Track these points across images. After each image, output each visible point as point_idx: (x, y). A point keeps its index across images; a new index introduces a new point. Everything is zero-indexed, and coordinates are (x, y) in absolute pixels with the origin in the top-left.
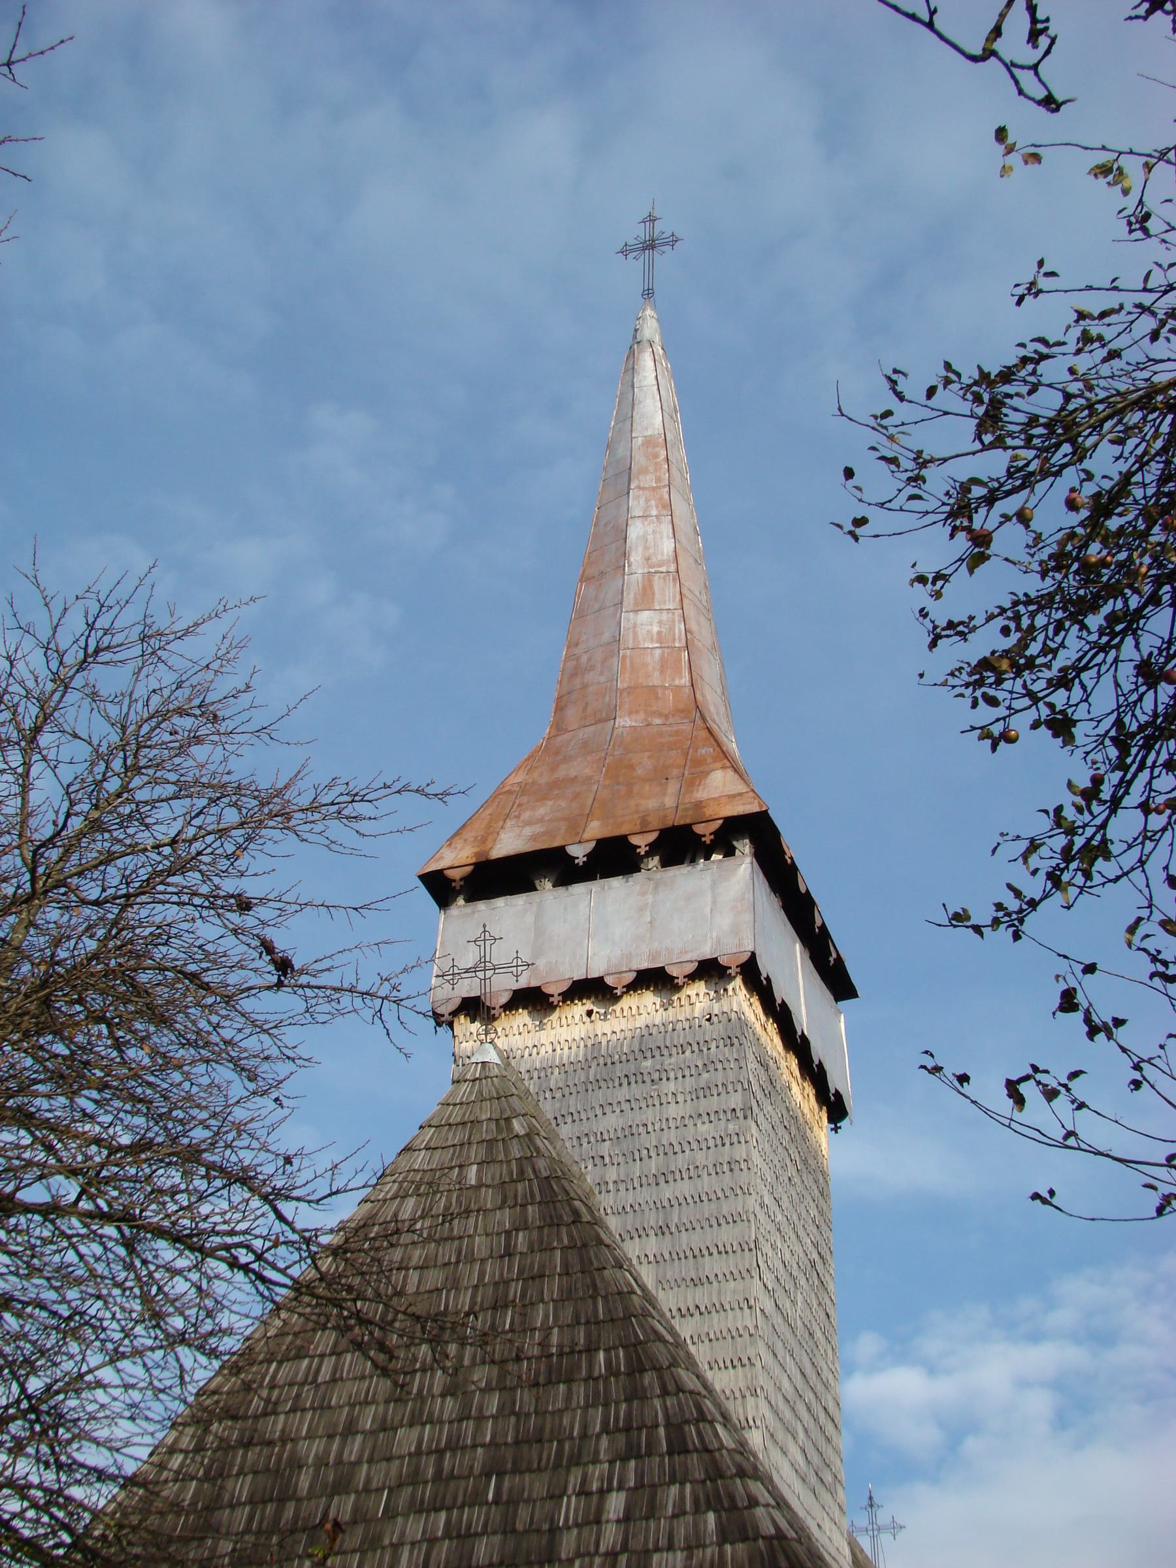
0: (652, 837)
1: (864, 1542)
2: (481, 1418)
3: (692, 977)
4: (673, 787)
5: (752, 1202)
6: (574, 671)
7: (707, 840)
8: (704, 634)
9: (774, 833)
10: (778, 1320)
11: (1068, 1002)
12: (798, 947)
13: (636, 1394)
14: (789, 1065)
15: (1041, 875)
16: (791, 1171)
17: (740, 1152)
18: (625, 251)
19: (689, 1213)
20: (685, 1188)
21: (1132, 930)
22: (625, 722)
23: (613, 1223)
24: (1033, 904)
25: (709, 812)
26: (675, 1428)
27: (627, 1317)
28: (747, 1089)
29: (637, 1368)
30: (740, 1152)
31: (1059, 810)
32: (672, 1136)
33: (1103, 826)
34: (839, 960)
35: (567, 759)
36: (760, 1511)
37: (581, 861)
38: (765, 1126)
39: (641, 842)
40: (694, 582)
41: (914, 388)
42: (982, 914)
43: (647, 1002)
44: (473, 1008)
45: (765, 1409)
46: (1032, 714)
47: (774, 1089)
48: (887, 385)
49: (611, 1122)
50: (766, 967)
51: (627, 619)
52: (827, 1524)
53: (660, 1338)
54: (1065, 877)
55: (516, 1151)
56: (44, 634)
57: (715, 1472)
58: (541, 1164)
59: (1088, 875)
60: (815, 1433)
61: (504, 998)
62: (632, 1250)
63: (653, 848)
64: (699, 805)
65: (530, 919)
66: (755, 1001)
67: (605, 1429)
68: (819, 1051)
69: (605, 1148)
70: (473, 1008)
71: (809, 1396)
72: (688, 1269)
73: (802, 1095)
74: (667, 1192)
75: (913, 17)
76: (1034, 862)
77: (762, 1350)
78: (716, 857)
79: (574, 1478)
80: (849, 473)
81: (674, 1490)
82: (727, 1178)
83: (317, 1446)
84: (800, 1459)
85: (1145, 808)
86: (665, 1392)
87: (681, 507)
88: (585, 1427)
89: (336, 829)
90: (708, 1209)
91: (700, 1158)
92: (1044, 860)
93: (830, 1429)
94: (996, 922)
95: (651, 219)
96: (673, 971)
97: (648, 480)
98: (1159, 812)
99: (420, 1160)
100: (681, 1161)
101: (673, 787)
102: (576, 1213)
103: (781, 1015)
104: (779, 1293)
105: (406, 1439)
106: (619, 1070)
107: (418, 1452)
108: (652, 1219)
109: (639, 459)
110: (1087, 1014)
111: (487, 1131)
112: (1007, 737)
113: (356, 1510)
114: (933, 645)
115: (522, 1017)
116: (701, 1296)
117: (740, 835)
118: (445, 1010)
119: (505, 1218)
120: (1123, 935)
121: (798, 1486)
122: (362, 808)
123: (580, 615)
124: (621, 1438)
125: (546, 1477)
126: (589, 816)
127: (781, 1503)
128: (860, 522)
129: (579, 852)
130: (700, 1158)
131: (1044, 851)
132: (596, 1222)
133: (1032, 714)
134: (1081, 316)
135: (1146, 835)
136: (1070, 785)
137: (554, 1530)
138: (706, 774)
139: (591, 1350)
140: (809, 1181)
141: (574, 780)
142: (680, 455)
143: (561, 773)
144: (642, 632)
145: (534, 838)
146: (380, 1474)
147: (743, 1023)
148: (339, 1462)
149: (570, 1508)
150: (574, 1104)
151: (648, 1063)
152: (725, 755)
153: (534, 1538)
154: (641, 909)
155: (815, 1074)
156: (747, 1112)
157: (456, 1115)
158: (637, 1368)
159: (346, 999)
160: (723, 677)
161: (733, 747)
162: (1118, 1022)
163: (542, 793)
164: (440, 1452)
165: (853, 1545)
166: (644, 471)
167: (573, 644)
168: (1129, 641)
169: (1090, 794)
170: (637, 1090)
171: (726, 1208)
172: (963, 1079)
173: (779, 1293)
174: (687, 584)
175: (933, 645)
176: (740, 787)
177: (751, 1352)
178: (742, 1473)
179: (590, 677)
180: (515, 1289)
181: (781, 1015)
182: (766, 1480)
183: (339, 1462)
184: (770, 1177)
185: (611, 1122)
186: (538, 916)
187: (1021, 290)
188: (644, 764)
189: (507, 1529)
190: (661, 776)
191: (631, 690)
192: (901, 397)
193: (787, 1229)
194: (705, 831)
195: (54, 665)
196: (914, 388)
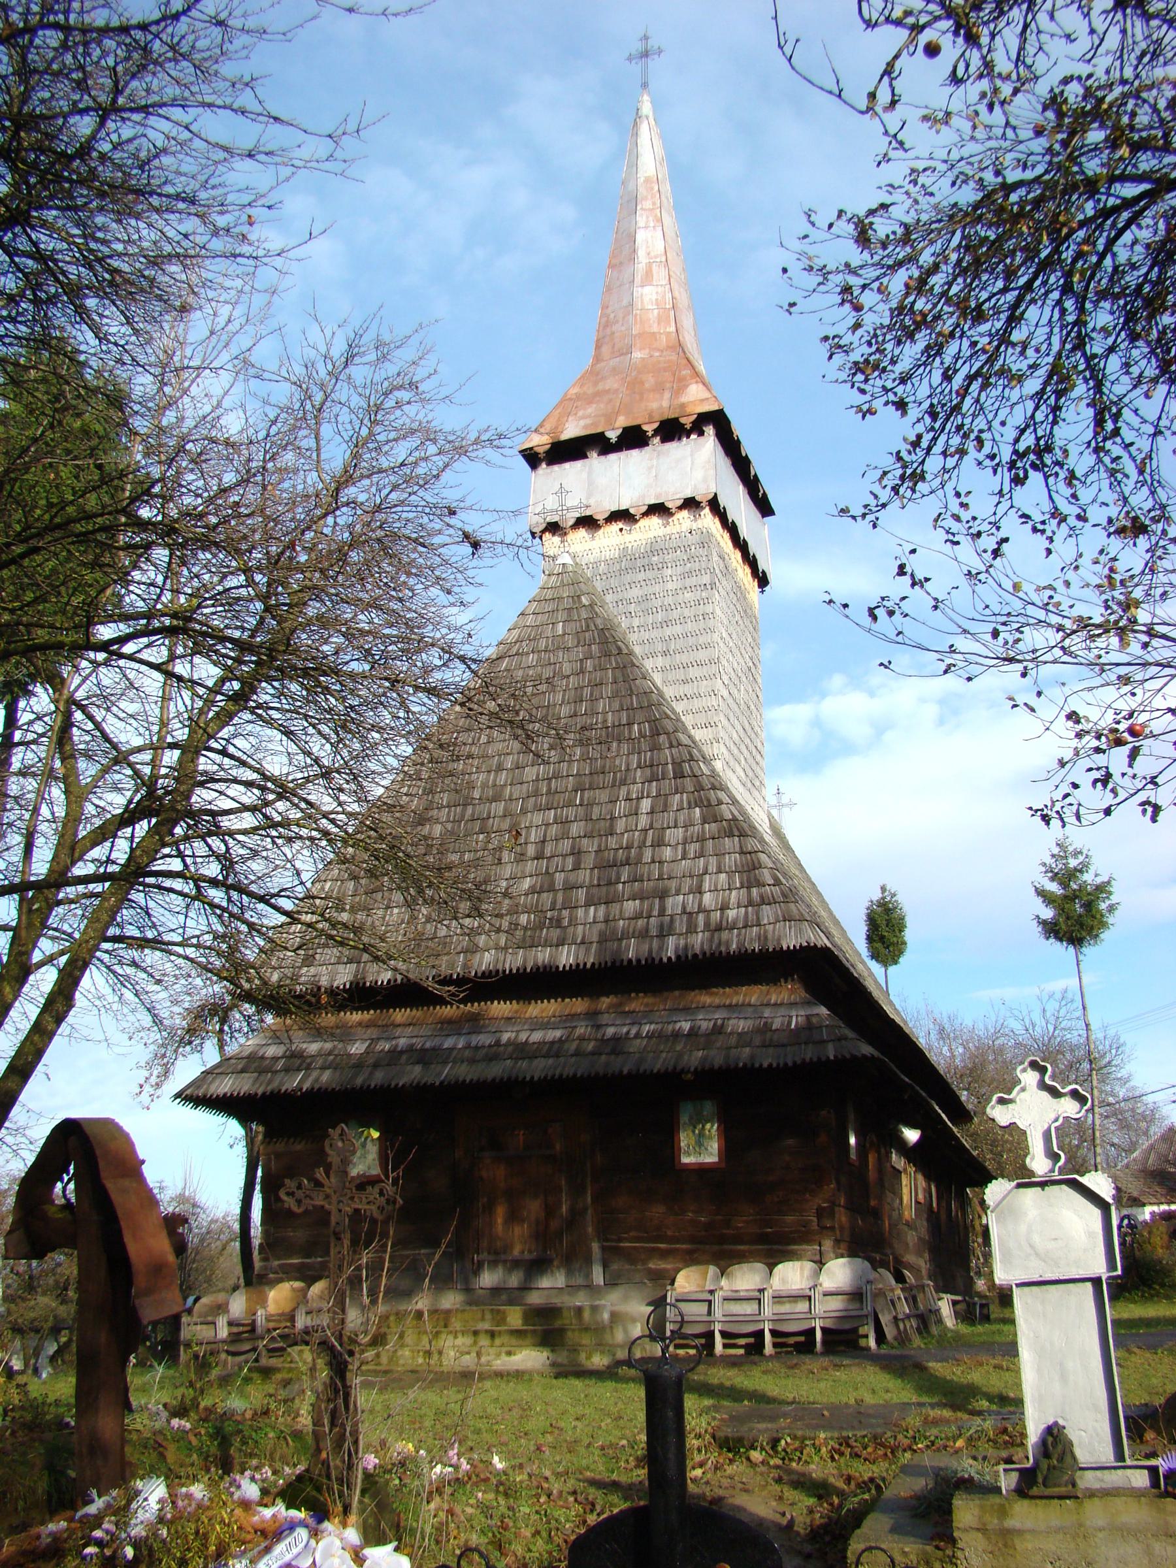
0: (656, 425)
1: (774, 812)
2: (570, 761)
3: (680, 508)
4: (667, 395)
5: (716, 637)
6: (606, 324)
7: (688, 427)
8: (683, 300)
9: (728, 422)
10: (730, 701)
11: (901, 570)
12: (741, 487)
13: (655, 748)
14: (737, 555)
15: (888, 488)
16: (738, 617)
17: (709, 608)
18: (630, 59)
19: (680, 644)
20: (678, 629)
21: (936, 520)
22: (637, 355)
23: (637, 650)
24: (884, 506)
25: (689, 410)
26: (677, 765)
27: (650, 706)
28: (713, 573)
29: (656, 733)
30: (709, 608)
31: (898, 452)
32: (669, 600)
33: (923, 462)
34: (764, 494)
35: (603, 379)
36: (723, 807)
37: (614, 440)
38: (723, 593)
39: (649, 429)
40: (676, 268)
41: (822, 221)
42: (857, 510)
43: (654, 523)
44: (553, 528)
45: (723, 749)
46: (884, 399)
47: (727, 571)
48: (805, 218)
49: (635, 592)
50: (722, 502)
51: (637, 291)
52: (756, 807)
53: (668, 717)
54: (902, 490)
55: (584, 614)
56: (323, 350)
57: (700, 788)
58: (599, 621)
59: (914, 491)
60: (751, 760)
61: (571, 522)
62: (648, 664)
63: (656, 432)
64: (683, 406)
65: (584, 475)
66: (717, 520)
67: (639, 766)
68: (753, 549)
69: (632, 608)
70: (553, 528)
71: (747, 741)
72: (680, 674)
73: (744, 573)
74: (668, 631)
75: (830, 92)
76: (884, 483)
77: (722, 718)
78: (693, 437)
79: (623, 792)
80: (785, 271)
81: (677, 796)
82: (702, 624)
83: (482, 777)
84: (742, 774)
85: (944, 454)
86: (671, 746)
87: (668, 220)
88: (628, 765)
89: (489, 453)
90: (691, 641)
91: (687, 612)
92: (891, 480)
93: (758, 757)
94: (864, 516)
95: (646, 38)
96: (669, 505)
97: (648, 204)
98: (952, 456)
99: (530, 620)
100: (675, 614)
101: (667, 395)
102: (619, 649)
103: (732, 529)
104: (731, 686)
105: (530, 773)
106: (639, 563)
107: (537, 780)
108: (660, 647)
109: (642, 191)
110: (912, 576)
111: (567, 603)
112: (871, 412)
113: (505, 809)
114: (830, 357)
115: (582, 532)
116: (688, 689)
117: (707, 423)
118: (537, 530)
119: (580, 652)
120: (931, 523)
121: (741, 788)
122: (504, 442)
123: (609, 289)
124: (648, 771)
125: (607, 791)
126: (618, 413)
127: (735, 802)
128: (792, 305)
129: (613, 435)
130: (687, 612)
131: (890, 476)
132: (631, 653)
133: (884, 399)
134: (913, 171)
135: (945, 470)
136: (905, 439)
137: (612, 819)
138: (686, 386)
139: (630, 724)
140: (748, 623)
141: (608, 392)
142: (667, 188)
143: (600, 387)
144: (646, 300)
145: (585, 427)
146: (518, 791)
147: (710, 535)
148: (495, 785)
149: (621, 807)
150: (613, 582)
151: (655, 559)
152: (697, 374)
153: (602, 823)
154: (650, 469)
155: (751, 561)
156: (713, 585)
157: (549, 594)
158: (656, 733)
159: (499, 547)
160: (695, 325)
161: (702, 368)
162: (927, 580)
163: (590, 400)
164: (549, 779)
165: (770, 817)
166: (645, 198)
167: (605, 307)
168: (938, 360)
169: (916, 444)
170: (650, 574)
171: (702, 640)
172: (845, 606)
173: (731, 686)
174: (673, 268)
175: (830, 357)
176: (707, 395)
177: (716, 719)
178: (714, 788)
179: (614, 328)
180: (587, 692)
181: (732, 529)
182: (723, 788)
183: (495, 785)
184: (725, 622)
185: (635, 592)
186: (590, 473)
187: (879, 158)
188: (650, 381)
189: (588, 819)
190: (659, 388)
191: (640, 335)
192: (813, 224)
193: (735, 650)
194: (687, 421)
195: (330, 367)
196: (822, 221)
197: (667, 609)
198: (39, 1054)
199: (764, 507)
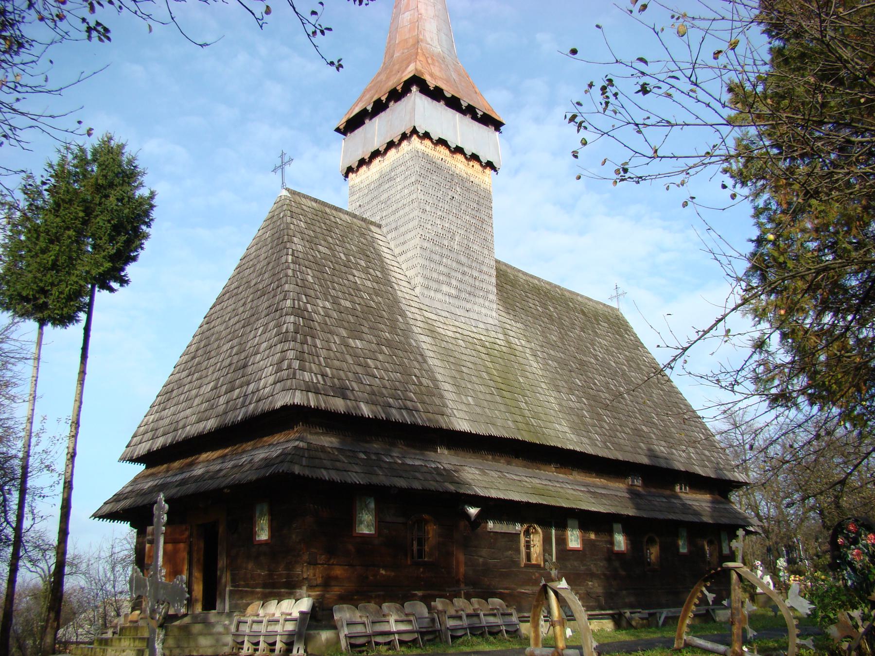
19: (402, 220)
74: (397, 215)
90: (407, 218)
197: (397, 202)
198: (61, 522)
199: (491, 122)
